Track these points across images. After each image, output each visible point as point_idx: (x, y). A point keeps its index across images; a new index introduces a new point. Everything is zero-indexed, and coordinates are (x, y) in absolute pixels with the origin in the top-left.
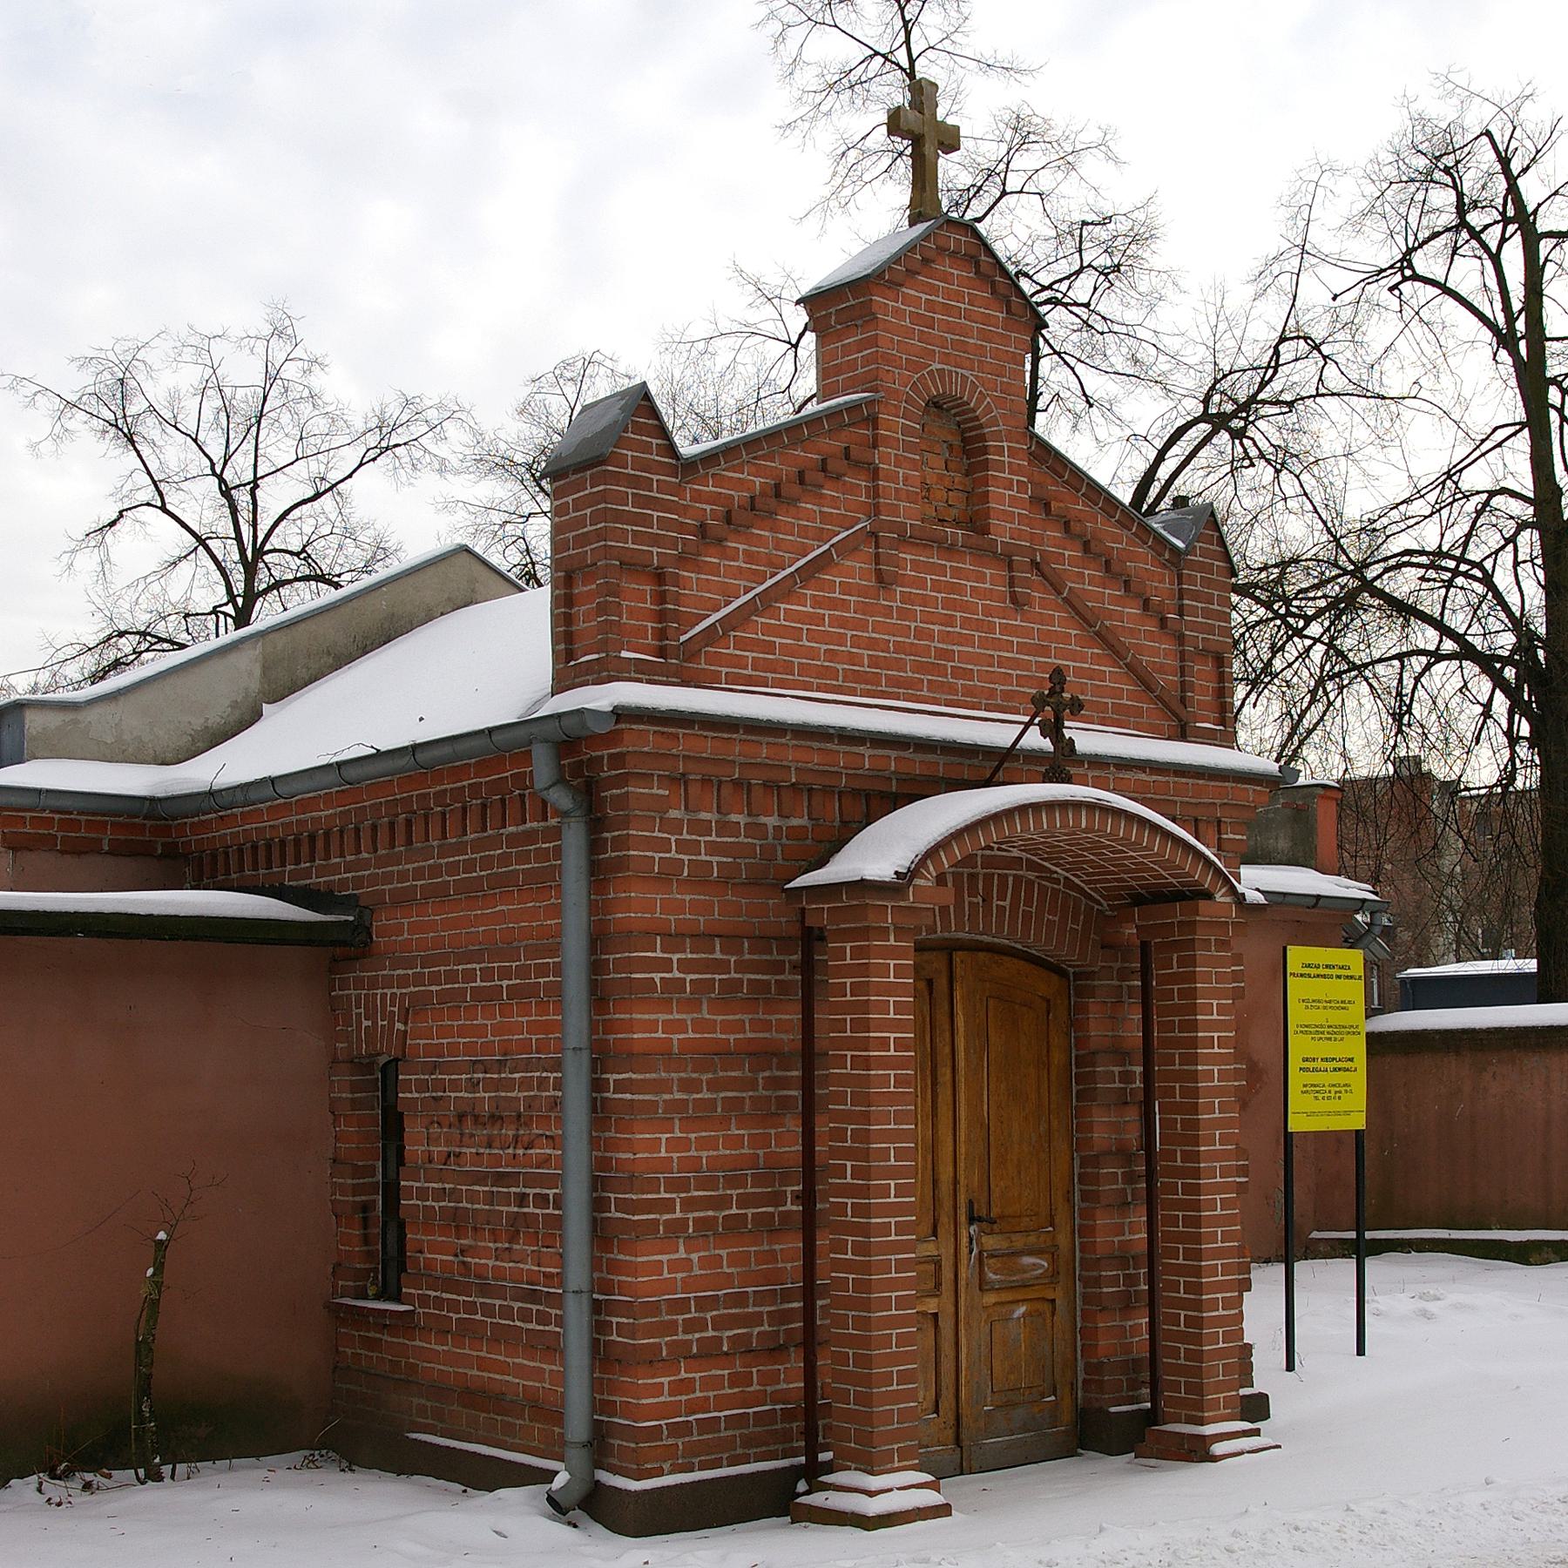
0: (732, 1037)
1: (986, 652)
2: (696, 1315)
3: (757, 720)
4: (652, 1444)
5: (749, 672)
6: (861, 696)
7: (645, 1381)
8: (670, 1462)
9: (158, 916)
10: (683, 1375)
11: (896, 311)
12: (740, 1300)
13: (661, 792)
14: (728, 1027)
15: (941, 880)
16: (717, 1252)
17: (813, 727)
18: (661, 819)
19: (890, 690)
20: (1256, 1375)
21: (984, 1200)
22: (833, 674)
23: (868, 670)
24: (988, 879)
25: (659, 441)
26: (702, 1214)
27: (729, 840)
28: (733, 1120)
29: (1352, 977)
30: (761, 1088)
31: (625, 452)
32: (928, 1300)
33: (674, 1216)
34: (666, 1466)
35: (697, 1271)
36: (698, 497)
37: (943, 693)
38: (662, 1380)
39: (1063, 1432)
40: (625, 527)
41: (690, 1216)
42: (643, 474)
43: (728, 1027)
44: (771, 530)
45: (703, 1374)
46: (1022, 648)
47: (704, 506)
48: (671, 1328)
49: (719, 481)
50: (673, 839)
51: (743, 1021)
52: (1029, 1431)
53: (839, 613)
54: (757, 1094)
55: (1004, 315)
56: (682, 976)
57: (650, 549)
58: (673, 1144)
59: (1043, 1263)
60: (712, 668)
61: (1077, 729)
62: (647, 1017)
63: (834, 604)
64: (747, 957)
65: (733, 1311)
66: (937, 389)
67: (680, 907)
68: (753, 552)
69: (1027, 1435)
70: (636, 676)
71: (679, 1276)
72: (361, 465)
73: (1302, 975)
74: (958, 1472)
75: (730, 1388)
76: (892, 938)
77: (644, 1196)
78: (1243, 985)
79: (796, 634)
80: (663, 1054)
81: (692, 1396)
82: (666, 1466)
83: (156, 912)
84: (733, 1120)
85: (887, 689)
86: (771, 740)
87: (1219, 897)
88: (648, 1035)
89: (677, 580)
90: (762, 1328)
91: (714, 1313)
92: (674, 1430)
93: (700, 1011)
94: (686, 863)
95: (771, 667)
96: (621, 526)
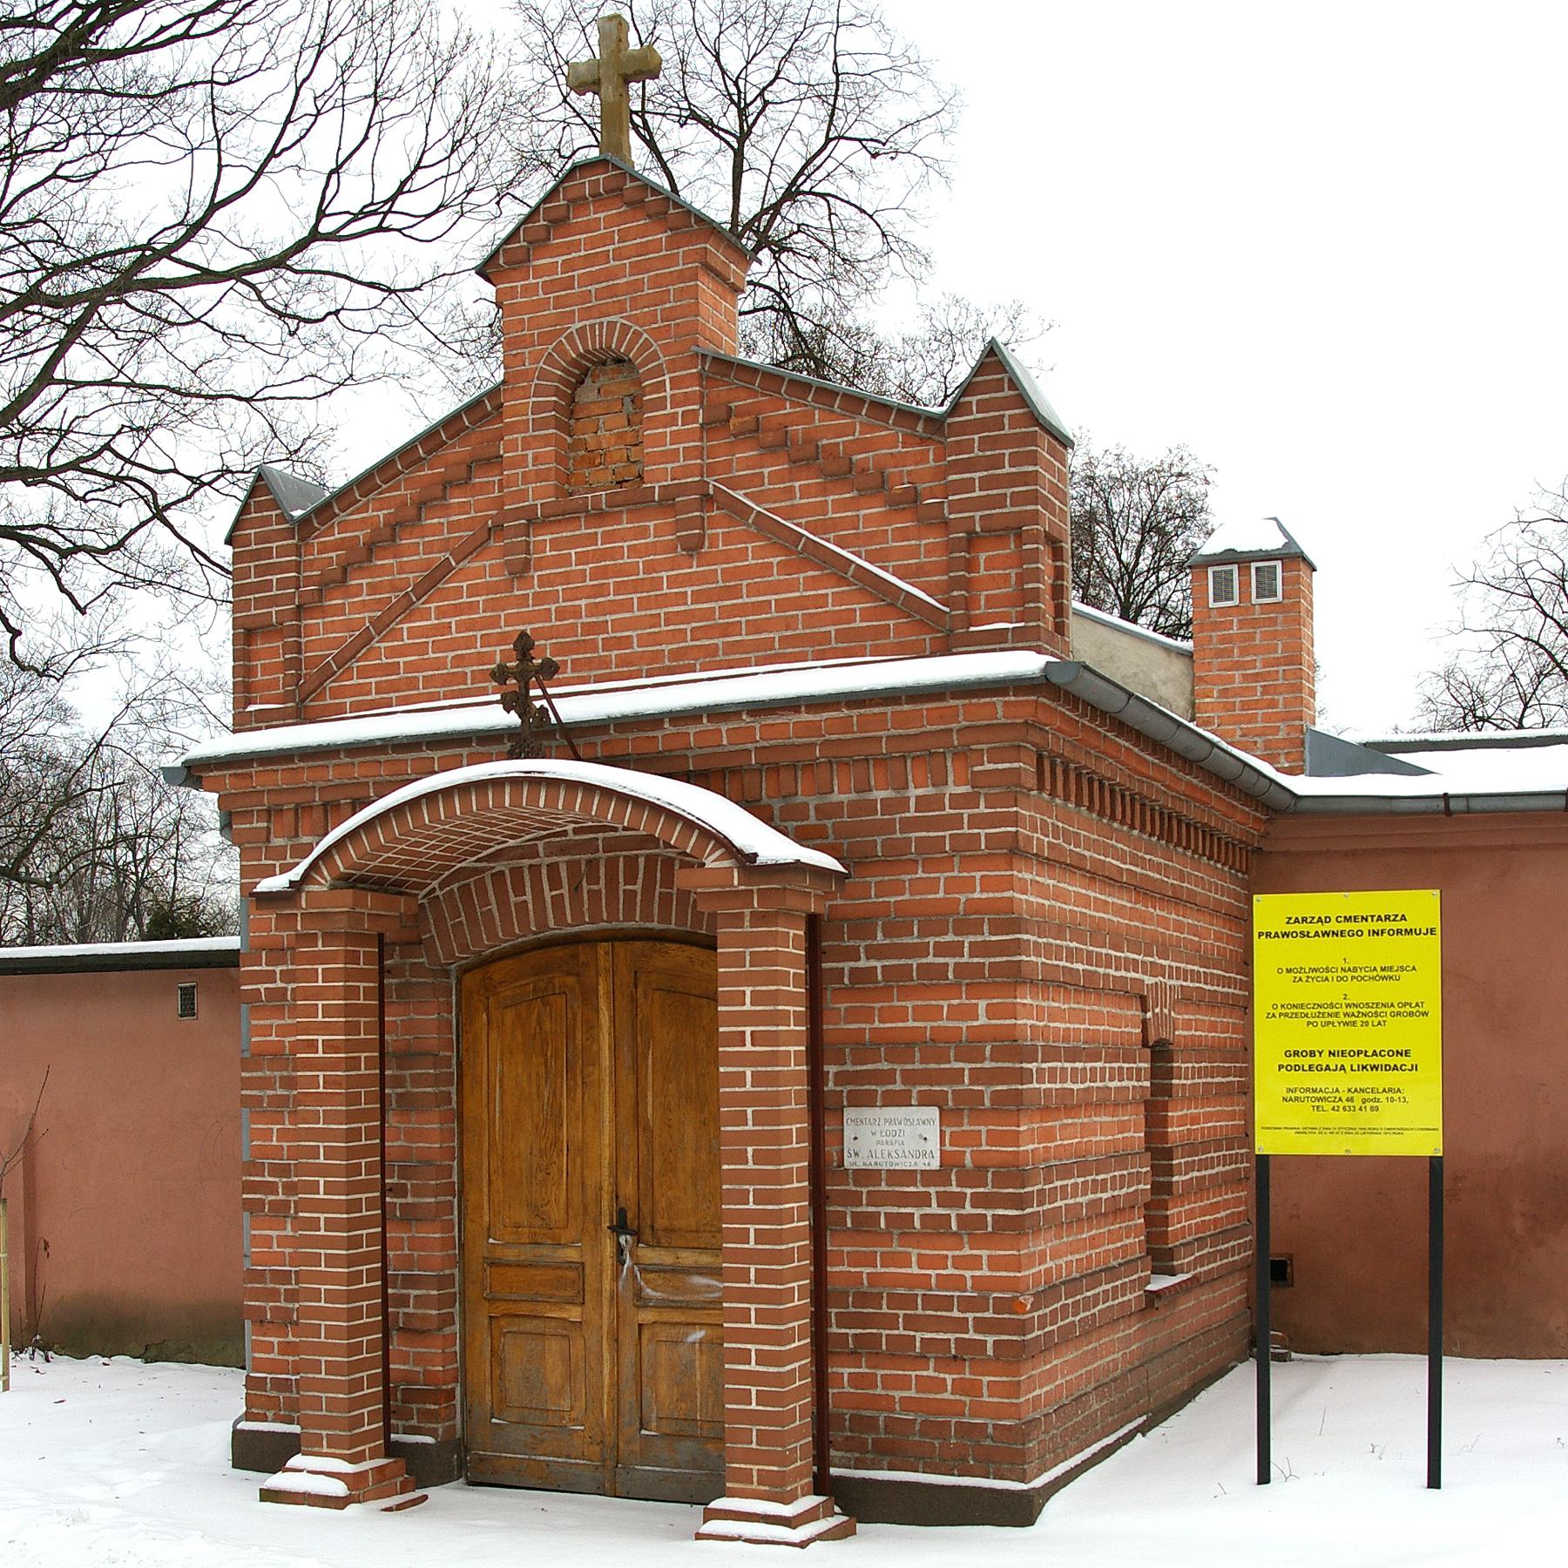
1: (649, 612)
5: (373, 696)
11: (528, 290)
17: (365, 742)
22: (412, 684)
24: (612, 864)
29: (1409, 932)
32: (568, 1307)
34: (270, 1414)
36: (324, 548)
37: (591, 670)
46: (698, 597)
47: (330, 555)
49: (344, 526)
50: (278, 864)
52: (700, 1468)
56: (283, 985)
58: (283, 1134)
62: (262, 1022)
63: (458, 610)
66: (575, 349)
69: (697, 1472)
71: (287, 1250)
73: (1285, 935)
76: (320, 943)
79: (423, 648)
82: (270, 1414)
87: (710, 863)
95: (393, 687)
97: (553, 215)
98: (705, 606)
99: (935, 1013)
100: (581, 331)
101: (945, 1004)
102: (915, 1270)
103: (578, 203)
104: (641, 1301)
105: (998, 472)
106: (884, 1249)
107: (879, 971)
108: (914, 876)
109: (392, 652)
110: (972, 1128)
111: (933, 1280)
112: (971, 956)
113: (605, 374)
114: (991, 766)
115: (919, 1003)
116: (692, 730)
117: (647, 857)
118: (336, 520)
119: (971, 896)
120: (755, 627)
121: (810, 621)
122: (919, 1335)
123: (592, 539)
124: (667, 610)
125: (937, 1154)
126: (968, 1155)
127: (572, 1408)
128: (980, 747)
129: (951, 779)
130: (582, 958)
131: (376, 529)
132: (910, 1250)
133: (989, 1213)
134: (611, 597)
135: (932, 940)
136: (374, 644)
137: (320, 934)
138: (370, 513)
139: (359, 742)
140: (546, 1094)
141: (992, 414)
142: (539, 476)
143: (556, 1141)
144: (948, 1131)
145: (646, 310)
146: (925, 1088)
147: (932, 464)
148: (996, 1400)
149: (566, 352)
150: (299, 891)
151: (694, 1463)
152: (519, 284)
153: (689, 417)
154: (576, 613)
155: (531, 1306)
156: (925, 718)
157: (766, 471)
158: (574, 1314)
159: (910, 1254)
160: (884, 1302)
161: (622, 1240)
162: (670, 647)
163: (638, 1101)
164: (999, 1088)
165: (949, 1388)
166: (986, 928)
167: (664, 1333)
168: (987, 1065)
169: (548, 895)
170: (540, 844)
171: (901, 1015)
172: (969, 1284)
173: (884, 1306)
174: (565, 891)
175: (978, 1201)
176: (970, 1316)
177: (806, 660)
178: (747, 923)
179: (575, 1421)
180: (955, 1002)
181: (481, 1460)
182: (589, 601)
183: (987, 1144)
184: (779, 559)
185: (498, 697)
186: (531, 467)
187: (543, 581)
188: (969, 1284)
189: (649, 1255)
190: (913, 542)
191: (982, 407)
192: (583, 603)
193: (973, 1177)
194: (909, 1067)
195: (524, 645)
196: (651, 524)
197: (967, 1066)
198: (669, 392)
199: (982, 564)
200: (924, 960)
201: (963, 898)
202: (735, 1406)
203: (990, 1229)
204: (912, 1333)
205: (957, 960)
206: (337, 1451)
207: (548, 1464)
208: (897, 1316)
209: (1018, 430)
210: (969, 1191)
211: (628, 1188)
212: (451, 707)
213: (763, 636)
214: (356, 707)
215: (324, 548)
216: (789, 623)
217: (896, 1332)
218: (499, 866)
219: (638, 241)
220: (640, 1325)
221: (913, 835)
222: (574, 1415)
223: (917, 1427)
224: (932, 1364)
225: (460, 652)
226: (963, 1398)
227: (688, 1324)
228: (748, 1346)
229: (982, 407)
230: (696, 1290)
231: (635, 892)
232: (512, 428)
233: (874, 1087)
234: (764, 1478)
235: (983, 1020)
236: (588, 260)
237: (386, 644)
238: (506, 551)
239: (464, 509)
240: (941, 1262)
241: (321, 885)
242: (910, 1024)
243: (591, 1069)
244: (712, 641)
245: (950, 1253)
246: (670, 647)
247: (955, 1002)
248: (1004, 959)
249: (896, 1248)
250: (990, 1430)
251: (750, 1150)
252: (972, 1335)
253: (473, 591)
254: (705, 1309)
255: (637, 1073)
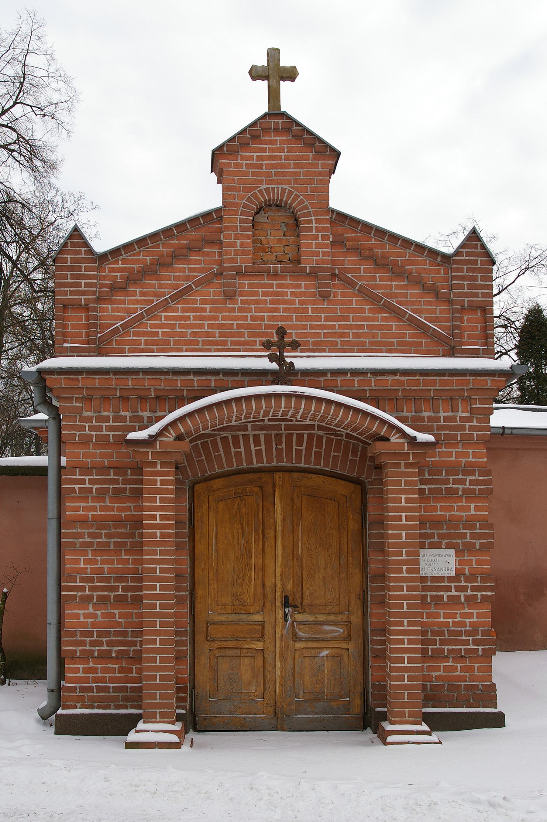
0: (123, 514)
1: (301, 323)
2: (97, 639)
3: (120, 368)
4: (71, 694)
5: (143, 346)
6: (156, 352)
7: (69, 666)
8: (80, 703)
9: (10, 466)
10: (91, 665)
11: (236, 165)
12: (124, 634)
13: (77, 404)
14: (120, 509)
15: (180, 438)
16: (112, 611)
18: (80, 416)
19: (233, 347)
20: (499, 701)
21: (298, 596)
22: (168, 343)
23: (219, 339)
24: (289, 437)
25: (86, 249)
26: (101, 593)
27: (120, 424)
28: (123, 552)
30: (137, 537)
31: (67, 256)
33: (85, 594)
34: (78, 705)
35: (100, 619)
36: (112, 270)
38: (79, 666)
39: (354, 717)
40: (66, 289)
41: (95, 594)
42: (77, 264)
43: (120, 509)
44: (157, 280)
45: (102, 666)
46: (327, 319)
48: (83, 643)
49: (124, 261)
50: (87, 425)
51: (131, 507)
52: (328, 714)
53: (199, 314)
54: (134, 540)
55: (314, 153)
56: (91, 486)
57: (80, 297)
58: (86, 562)
59: (340, 630)
60: (120, 347)
61: (335, 356)
64: (129, 477)
65: (119, 638)
66: (264, 197)
67: (94, 455)
68: (145, 291)
70: (71, 354)
71: (90, 620)
72: (518, 276)
74: (275, 729)
75: (118, 673)
77: (68, 584)
78: (491, 487)
79: (173, 326)
80: (84, 522)
81: (96, 675)
83: (9, 465)
84: (123, 552)
85: (231, 347)
86: (134, 377)
87: (393, 439)
88: (75, 513)
89: (95, 309)
90: (136, 648)
91: (108, 639)
92: (82, 689)
93: (105, 502)
94: (95, 435)
95: (156, 343)
96: (63, 289)
97: (254, 134)
98: (331, 323)
99: (451, 509)
100: (267, 190)
101: (455, 505)
102: (442, 619)
103: (266, 130)
104: (295, 638)
105: (475, 282)
106: (427, 611)
107: (427, 490)
108: (440, 450)
109: (153, 326)
110: (469, 558)
111: (451, 624)
112: (470, 485)
113: (271, 211)
114: (480, 406)
115: (443, 504)
116: (339, 379)
117: (308, 434)
118: (121, 257)
119: (467, 460)
120: (356, 335)
121: (384, 335)
122: (446, 648)
123: (271, 286)
124: (311, 323)
125: (454, 569)
126: (467, 570)
127: (256, 691)
128: (475, 397)
129: (460, 409)
130: (264, 479)
131: (146, 265)
132: (439, 611)
133: (479, 594)
134: (281, 314)
135: (451, 478)
136: (144, 321)
137: (159, 462)
138: (141, 257)
139: (152, 369)
140: (242, 542)
141: (472, 258)
142: (243, 253)
143: (248, 565)
144: (457, 559)
145: (302, 186)
146: (449, 541)
147: (443, 275)
148: (481, 674)
149: (259, 198)
150: (156, 440)
151: (325, 712)
152: (232, 162)
153: (324, 237)
154: (262, 318)
155: (234, 643)
156: (454, 383)
157: (362, 267)
158: (259, 646)
159: (440, 612)
160: (429, 634)
161: (287, 610)
162: (313, 340)
163: (295, 545)
164: (483, 541)
165: (459, 670)
166: (477, 473)
167: (307, 653)
168: (477, 531)
169: (253, 449)
170: (249, 425)
171: (435, 509)
172: (468, 625)
173: (429, 636)
174: (263, 447)
175: (473, 589)
176: (471, 638)
177: (411, 353)
178: (403, 467)
179: (257, 697)
180: (460, 504)
181: (205, 719)
182: (269, 314)
183: (476, 565)
184: (369, 307)
185: (266, 354)
186: (239, 248)
187: (243, 302)
188: (468, 625)
189: (300, 617)
190: (434, 307)
191: (468, 254)
192: (266, 314)
193: (471, 578)
194: (441, 532)
195: (282, 332)
196: (303, 283)
197: (468, 532)
198: (314, 225)
199: (465, 320)
200: (448, 486)
201: (464, 461)
202: (396, 683)
203: (479, 601)
204: (443, 647)
205: (463, 486)
206: (166, 720)
207: (244, 718)
208: (436, 640)
209: (484, 267)
210: (469, 585)
211: (290, 586)
212: (220, 356)
213: (361, 340)
214: (131, 351)
215: (112, 270)
216: (374, 336)
217: (436, 647)
218: (225, 434)
219: (297, 154)
220: (295, 649)
221: (443, 432)
222: (256, 694)
223: (446, 688)
224: (451, 660)
225: (195, 330)
226: (465, 674)
227: (322, 648)
228: (403, 655)
229: (468, 254)
230: (328, 632)
231: (302, 450)
232: (228, 228)
233: (424, 540)
234: (411, 714)
235: (473, 512)
236: (270, 158)
237: (151, 322)
238: (224, 285)
239: (197, 262)
240: (454, 616)
241: (170, 437)
242: (439, 513)
243: (269, 531)
244: (335, 339)
245: (458, 612)
246: (313, 340)
247: (460, 504)
248: (485, 487)
249: (433, 610)
250: (480, 687)
251: (404, 567)
252: (471, 646)
253: (203, 302)
254: (331, 641)
255: (293, 533)
